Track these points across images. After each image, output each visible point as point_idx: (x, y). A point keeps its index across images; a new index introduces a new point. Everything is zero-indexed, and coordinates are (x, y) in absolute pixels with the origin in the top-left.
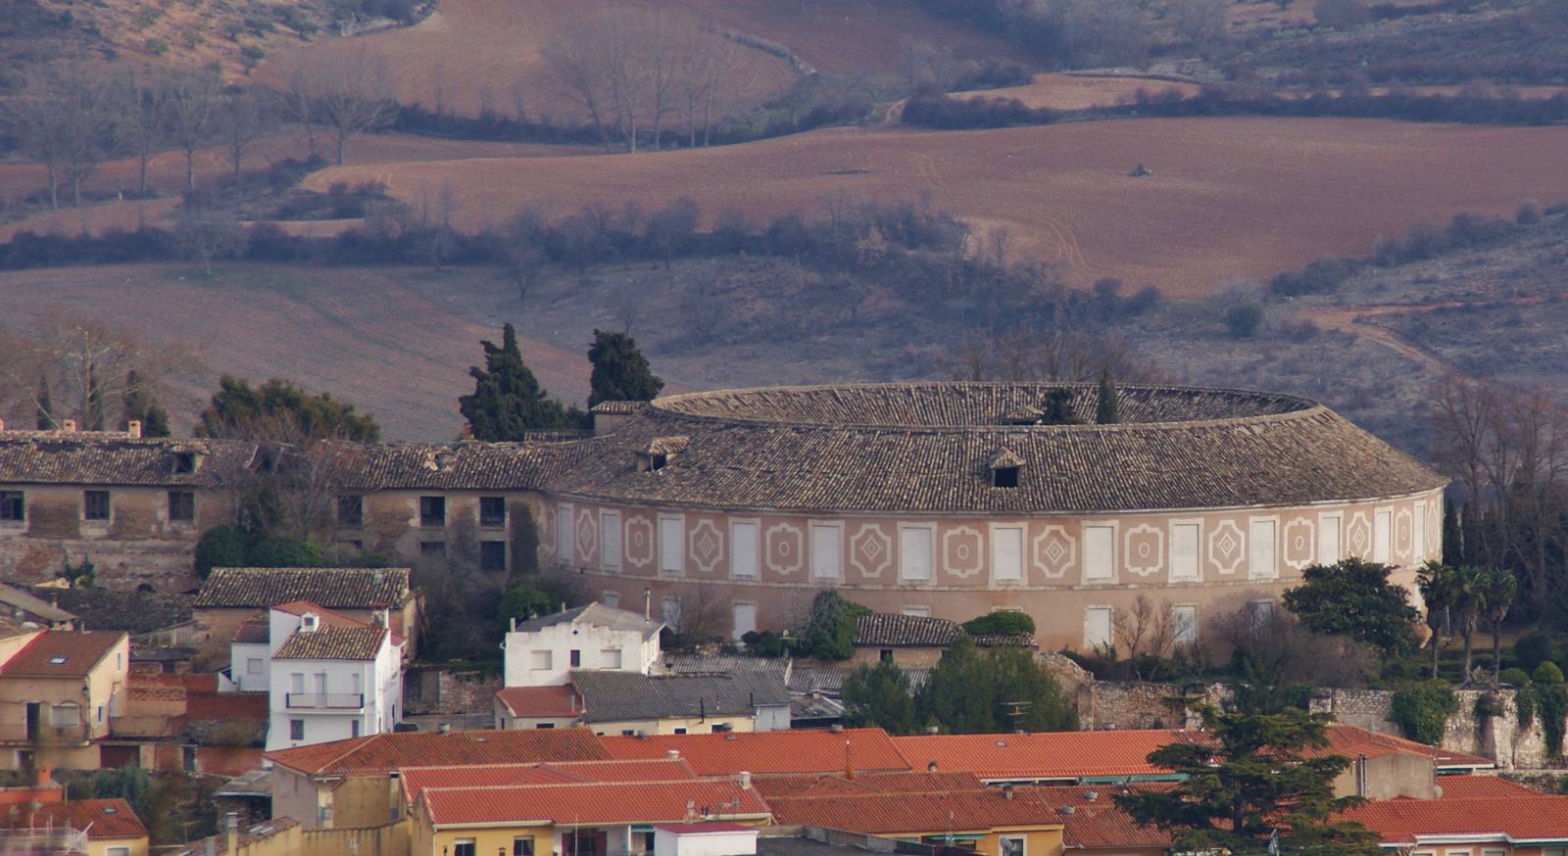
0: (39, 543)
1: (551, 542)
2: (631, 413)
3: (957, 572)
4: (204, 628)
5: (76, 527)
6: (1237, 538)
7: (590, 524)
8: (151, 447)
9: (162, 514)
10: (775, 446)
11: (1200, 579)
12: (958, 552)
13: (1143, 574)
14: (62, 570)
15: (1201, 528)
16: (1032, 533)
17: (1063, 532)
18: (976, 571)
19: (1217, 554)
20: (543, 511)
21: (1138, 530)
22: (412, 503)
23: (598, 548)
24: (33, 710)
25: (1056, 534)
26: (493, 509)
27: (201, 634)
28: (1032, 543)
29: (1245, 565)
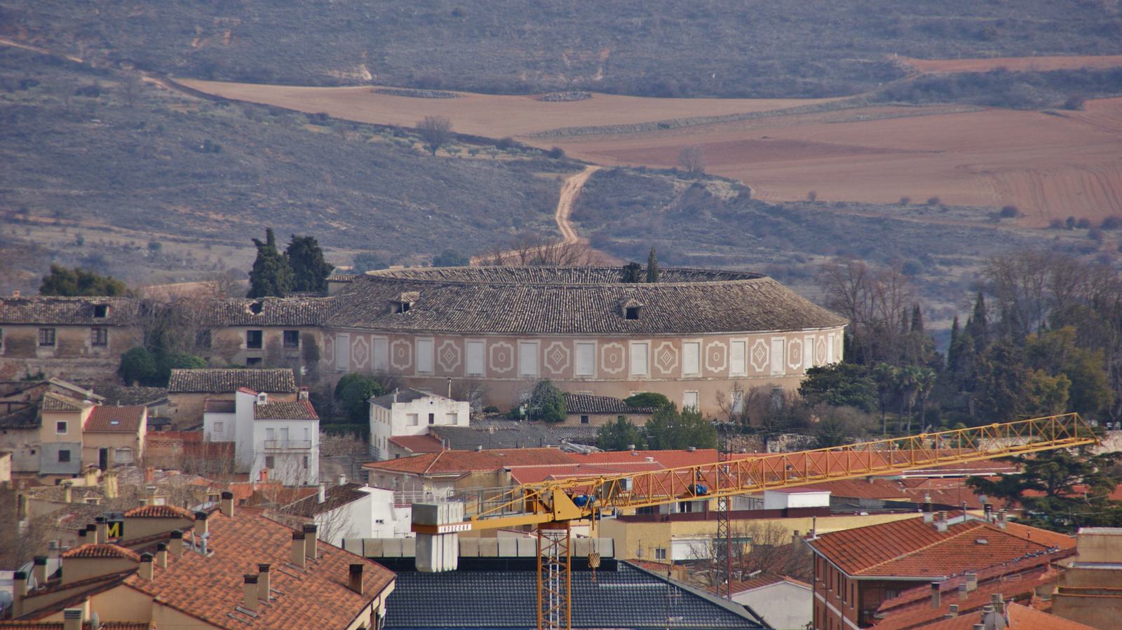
1: (328, 357)
2: (351, 282)
3: (610, 370)
4: (175, 405)
5: (34, 350)
6: (765, 349)
7: (363, 345)
8: (74, 302)
9: (88, 343)
10: (482, 296)
11: (745, 375)
13: (716, 371)
14: (25, 377)
15: (747, 344)
16: (654, 346)
17: (671, 346)
18: (621, 370)
19: (755, 360)
20: (322, 338)
21: (713, 345)
22: (242, 334)
23: (370, 358)
25: (667, 347)
26: (291, 337)
27: (173, 409)
29: (769, 366)
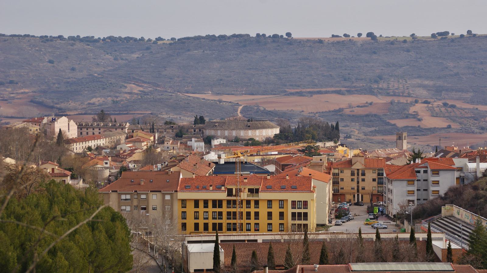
0: (160, 134)
22: (193, 130)
24: (173, 147)
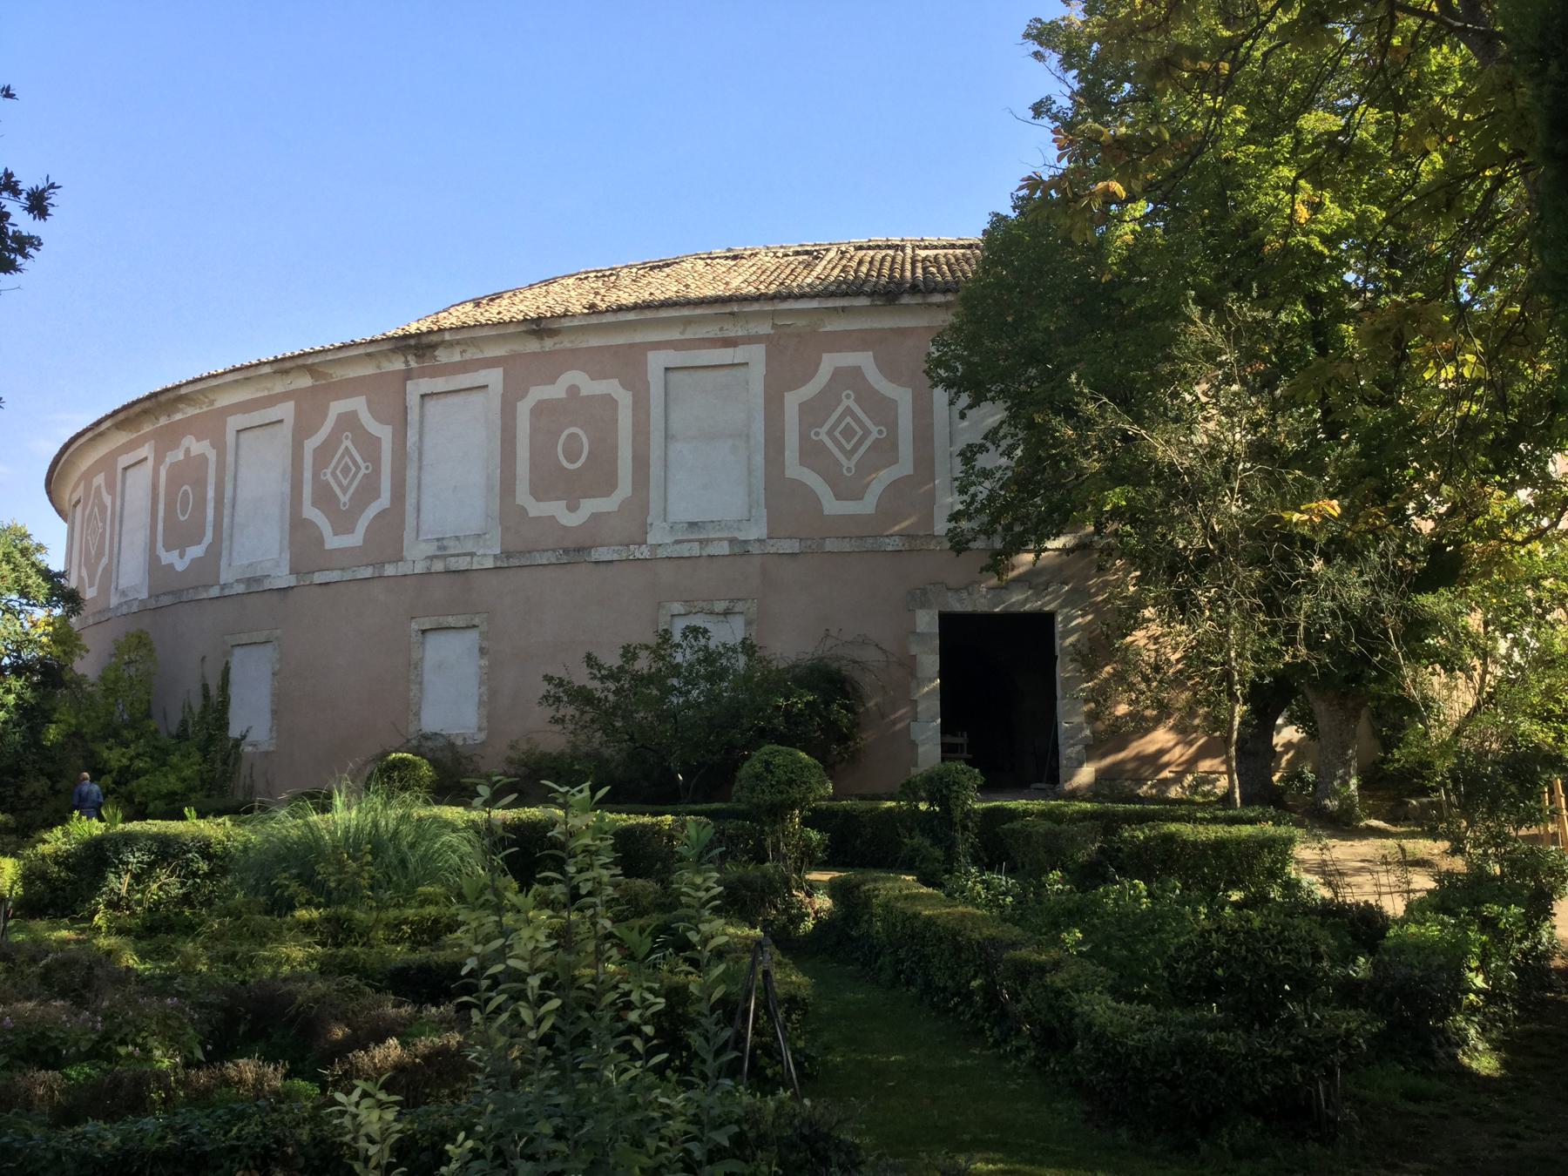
12: (561, 458)
28: (635, 483)
